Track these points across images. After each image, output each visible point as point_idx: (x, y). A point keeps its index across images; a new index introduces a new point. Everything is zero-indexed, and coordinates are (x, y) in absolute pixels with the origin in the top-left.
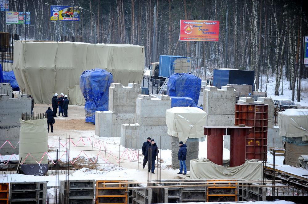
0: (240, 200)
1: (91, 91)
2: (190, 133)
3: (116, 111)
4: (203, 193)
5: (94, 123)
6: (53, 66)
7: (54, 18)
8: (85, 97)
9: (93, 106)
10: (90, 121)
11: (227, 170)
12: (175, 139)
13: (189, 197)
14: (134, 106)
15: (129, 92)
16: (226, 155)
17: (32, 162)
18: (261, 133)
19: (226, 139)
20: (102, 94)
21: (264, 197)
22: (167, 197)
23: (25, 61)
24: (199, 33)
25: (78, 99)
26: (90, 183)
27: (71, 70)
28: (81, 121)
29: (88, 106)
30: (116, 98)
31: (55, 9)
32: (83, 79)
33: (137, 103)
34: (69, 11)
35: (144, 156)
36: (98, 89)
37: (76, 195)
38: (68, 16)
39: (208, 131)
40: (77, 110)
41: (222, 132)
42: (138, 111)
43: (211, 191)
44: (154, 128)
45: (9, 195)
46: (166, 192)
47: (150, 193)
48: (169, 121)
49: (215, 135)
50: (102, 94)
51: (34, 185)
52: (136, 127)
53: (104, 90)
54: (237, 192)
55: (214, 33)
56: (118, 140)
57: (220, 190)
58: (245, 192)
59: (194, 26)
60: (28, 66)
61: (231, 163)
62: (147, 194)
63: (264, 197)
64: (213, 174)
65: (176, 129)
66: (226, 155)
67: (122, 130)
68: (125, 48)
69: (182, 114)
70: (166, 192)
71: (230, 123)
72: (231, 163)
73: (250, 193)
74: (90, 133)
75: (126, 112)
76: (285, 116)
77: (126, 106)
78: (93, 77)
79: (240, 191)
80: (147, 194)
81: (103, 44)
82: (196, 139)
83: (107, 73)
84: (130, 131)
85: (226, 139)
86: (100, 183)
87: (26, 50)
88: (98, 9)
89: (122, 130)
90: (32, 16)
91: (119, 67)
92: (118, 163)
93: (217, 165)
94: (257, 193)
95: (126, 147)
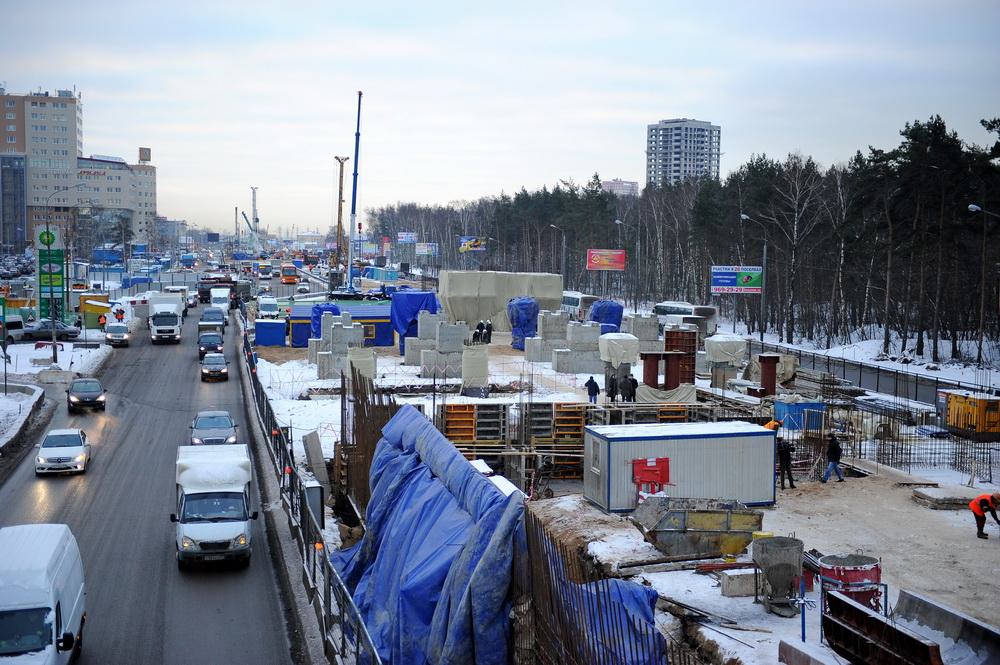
0: (690, 421)
1: (518, 318)
2: (623, 357)
3: (546, 337)
4: (655, 415)
5: (523, 350)
6: (476, 294)
7: (463, 249)
8: (512, 323)
9: (520, 332)
10: (519, 347)
11: (662, 394)
12: (609, 364)
13: (642, 419)
14: (565, 332)
15: (558, 318)
16: (661, 380)
17: (475, 385)
18: (691, 359)
19: (662, 364)
20: (529, 321)
21: (715, 419)
22: (624, 419)
23: (450, 290)
24: (606, 262)
25: (500, 324)
26: (549, 405)
27: (494, 298)
28: (507, 346)
29: (515, 332)
30: (545, 325)
31: (463, 240)
32: (510, 306)
33: (568, 330)
34: (476, 241)
35: (281, 425)
36: (525, 316)
37: (536, 416)
38: (476, 246)
39: (644, 357)
40: (503, 337)
41: (658, 357)
42: (569, 337)
43: (662, 413)
44: (585, 354)
45: (475, 416)
46: (624, 414)
47: (608, 415)
48: (603, 347)
49: (650, 361)
50: (529, 321)
51: (497, 407)
52: (567, 353)
53: (530, 317)
54: (687, 414)
55: (621, 262)
56: (548, 365)
57: (672, 413)
58: (695, 413)
59: (601, 255)
60: (453, 294)
61: (666, 387)
62: (605, 416)
63: (715, 419)
64: (647, 396)
65: (610, 355)
66: (661, 380)
67: (554, 356)
68: (545, 277)
69: (615, 340)
70: (624, 414)
71: (660, 348)
72: (666, 387)
73: (699, 414)
74: (519, 359)
75: (555, 338)
76: (712, 342)
77: (557, 331)
78: (520, 305)
79: (690, 413)
80: (605, 416)
81: (523, 273)
82: (629, 364)
83: (533, 300)
84: (561, 356)
85: (662, 364)
86: (559, 405)
87: (452, 280)
88: (886, 254)
89: (554, 356)
90: (440, 246)
91: (539, 294)
92: (555, 388)
93: (653, 389)
94: (707, 414)
95: (558, 371)
